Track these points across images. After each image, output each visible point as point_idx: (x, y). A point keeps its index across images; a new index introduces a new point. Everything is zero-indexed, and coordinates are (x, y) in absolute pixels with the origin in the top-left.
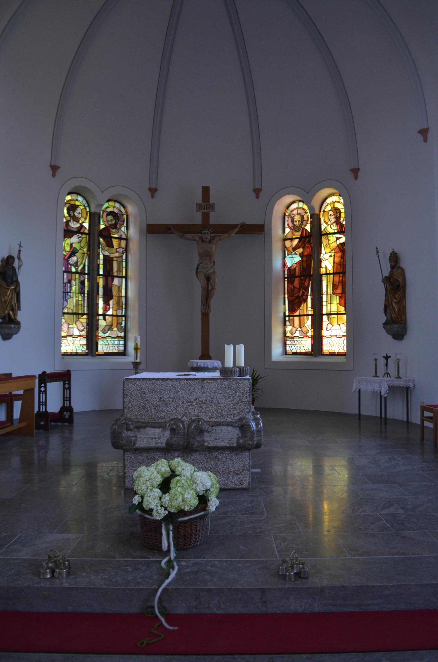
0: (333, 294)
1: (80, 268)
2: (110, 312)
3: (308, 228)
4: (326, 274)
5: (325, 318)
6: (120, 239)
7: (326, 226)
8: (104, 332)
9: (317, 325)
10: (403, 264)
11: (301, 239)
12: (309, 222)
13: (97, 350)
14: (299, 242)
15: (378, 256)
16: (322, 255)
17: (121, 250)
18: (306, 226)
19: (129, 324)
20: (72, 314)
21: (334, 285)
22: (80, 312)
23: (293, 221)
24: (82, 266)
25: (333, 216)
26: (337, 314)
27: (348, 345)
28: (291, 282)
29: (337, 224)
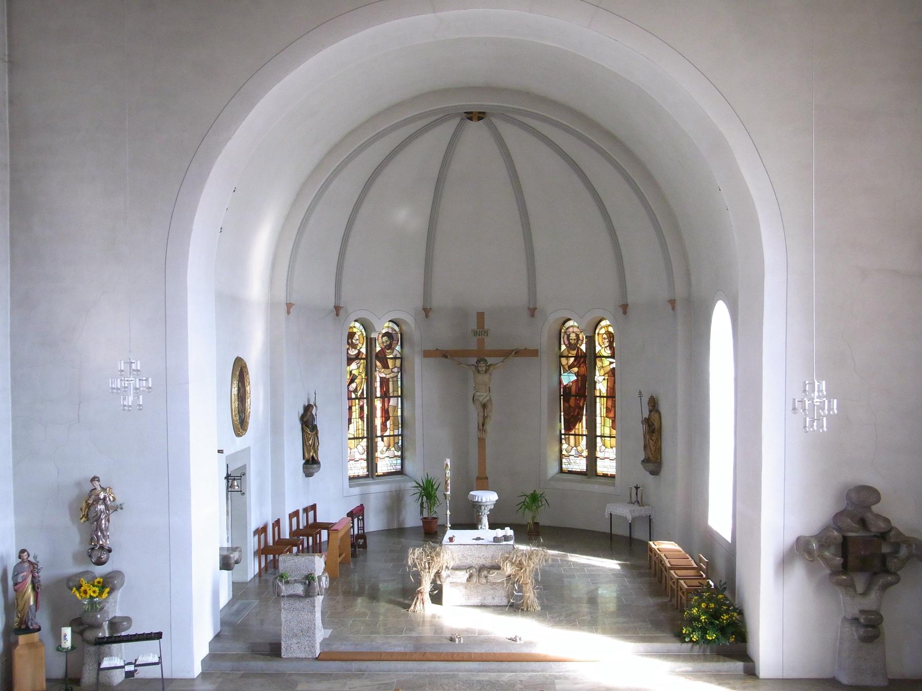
2: (387, 433)
3: (583, 347)
4: (600, 397)
5: (599, 439)
6: (395, 358)
9: (592, 446)
10: (663, 407)
11: (576, 357)
17: (396, 370)
19: (405, 444)
26: (610, 437)
27: (618, 467)
28: (566, 400)
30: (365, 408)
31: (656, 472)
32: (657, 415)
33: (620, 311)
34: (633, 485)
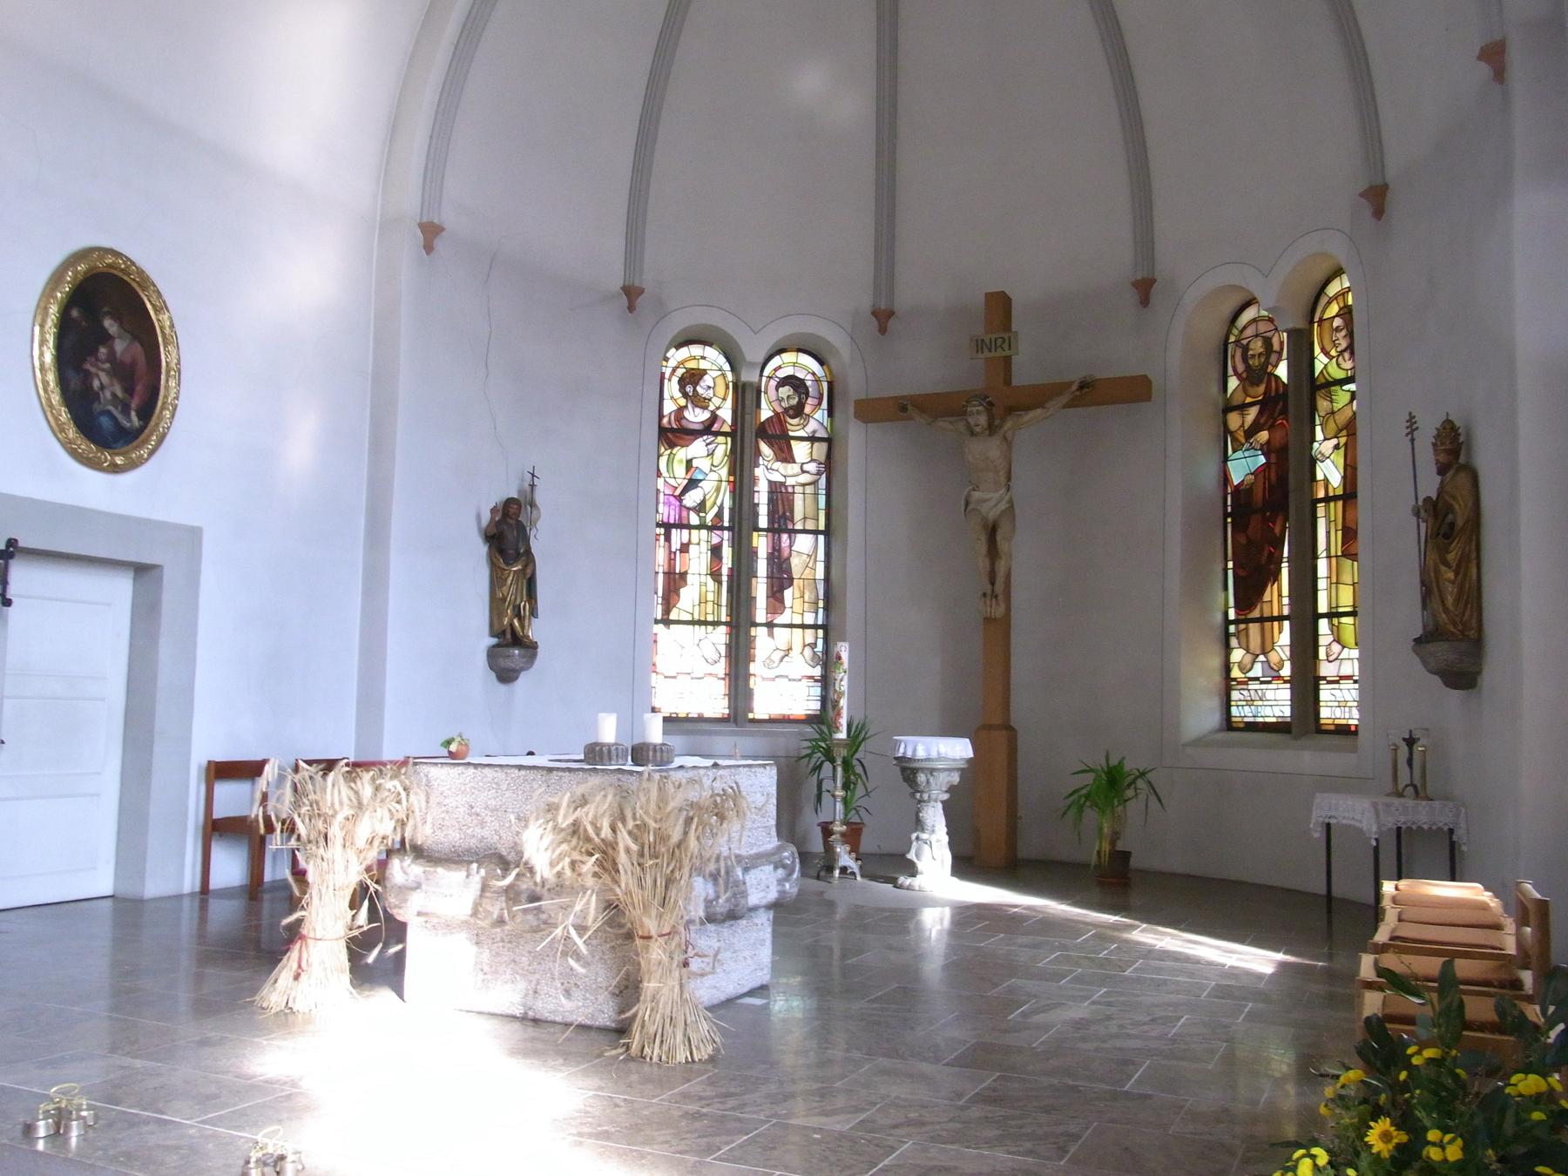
0: (1344, 555)
3: (1282, 371)
4: (1327, 499)
5: (1323, 625)
6: (812, 439)
7: (1326, 360)
8: (768, 664)
10: (1486, 458)
11: (1266, 404)
14: (1260, 413)
15: (1412, 440)
16: (1316, 445)
17: (812, 467)
18: (1276, 366)
22: (710, 618)
23: (1245, 358)
24: (715, 510)
25: (1344, 333)
30: (727, 552)
31: (1462, 675)
32: (1463, 479)
33: (1367, 210)
34: (1397, 737)
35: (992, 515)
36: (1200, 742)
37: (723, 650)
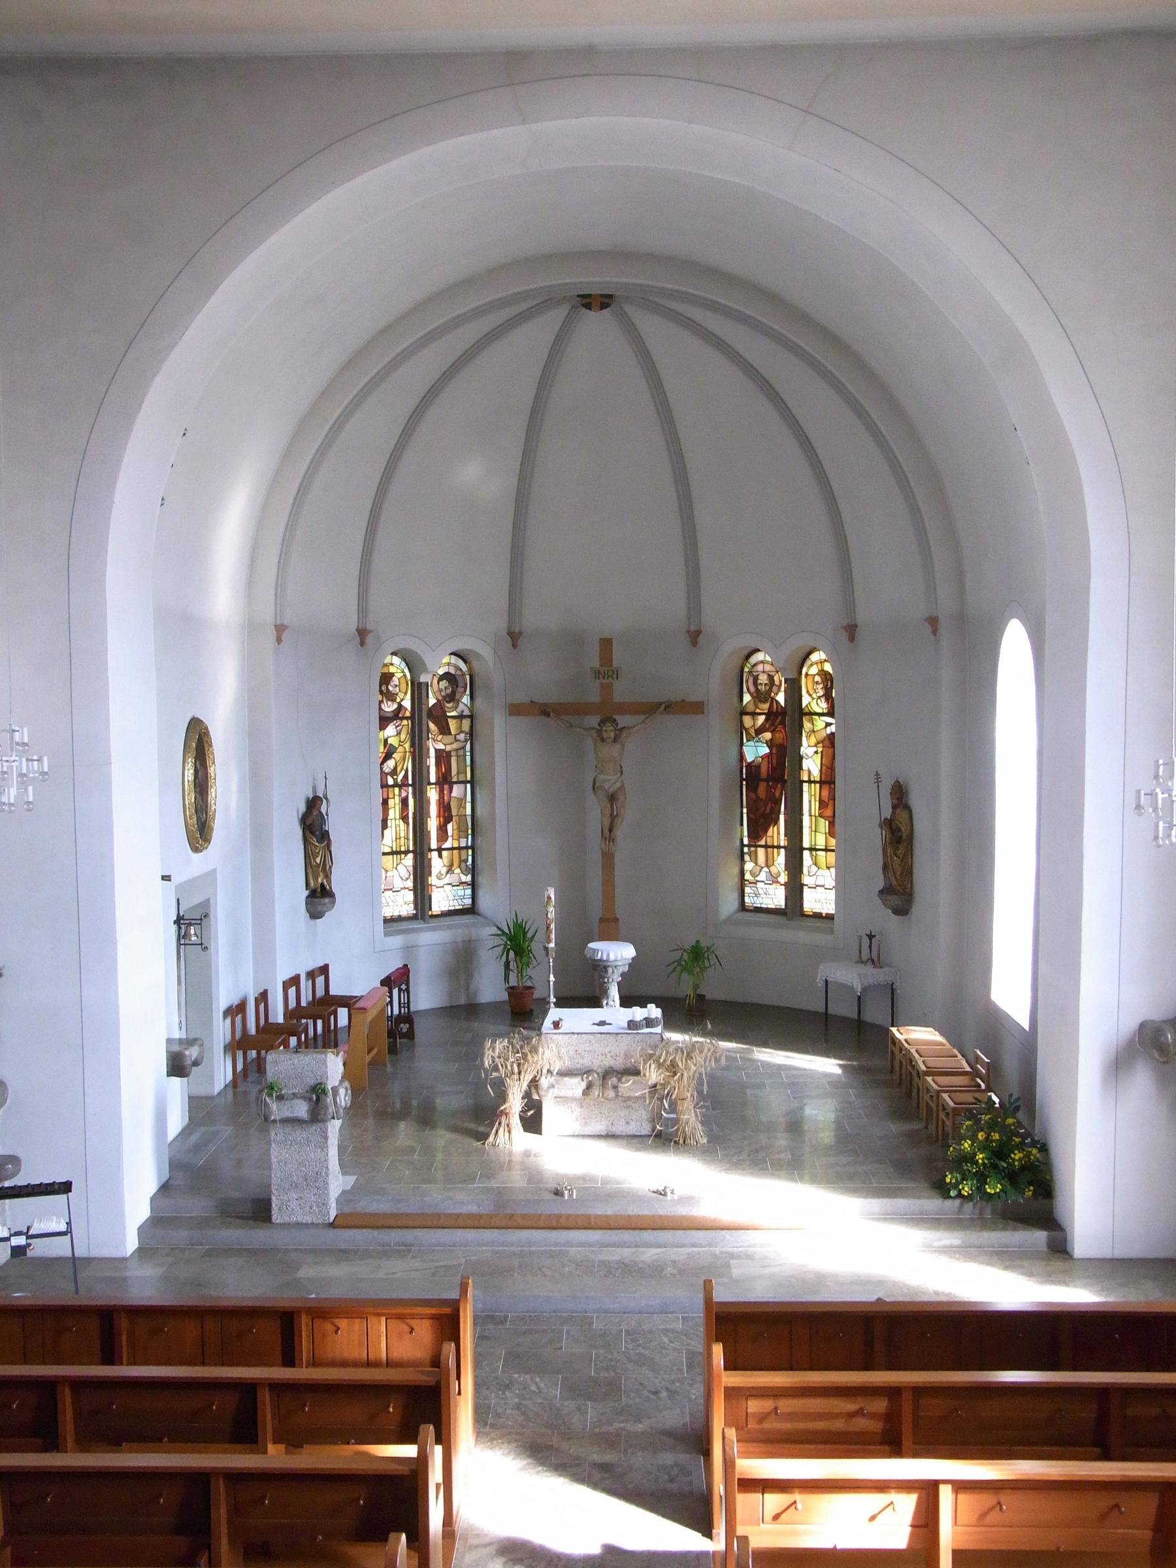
1: (400, 778)
2: (447, 845)
3: (781, 698)
5: (806, 854)
6: (461, 717)
7: (810, 699)
10: (916, 801)
11: (769, 715)
12: (783, 689)
13: (430, 909)
14: (766, 720)
17: (462, 737)
19: (479, 861)
20: (392, 853)
21: (821, 801)
22: (403, 849)
23: (755, 683)
24: (403, 773)
28: (752, 788)
29: (827, 700)
30: (411, 801)
32: (905, 815)
33: (844, 636)
35: (612, 790)
36: (728, 921)
37: (411, 869)
